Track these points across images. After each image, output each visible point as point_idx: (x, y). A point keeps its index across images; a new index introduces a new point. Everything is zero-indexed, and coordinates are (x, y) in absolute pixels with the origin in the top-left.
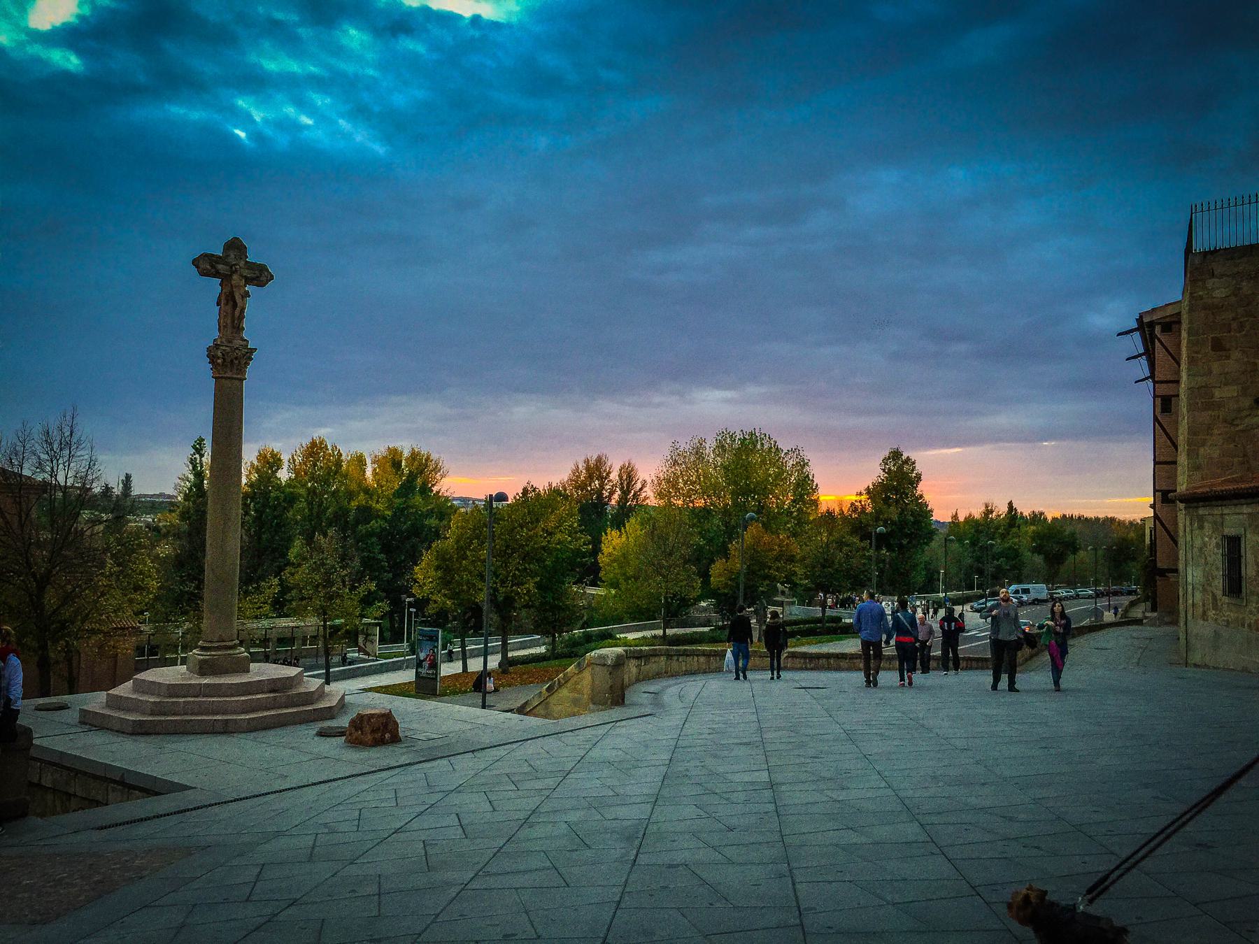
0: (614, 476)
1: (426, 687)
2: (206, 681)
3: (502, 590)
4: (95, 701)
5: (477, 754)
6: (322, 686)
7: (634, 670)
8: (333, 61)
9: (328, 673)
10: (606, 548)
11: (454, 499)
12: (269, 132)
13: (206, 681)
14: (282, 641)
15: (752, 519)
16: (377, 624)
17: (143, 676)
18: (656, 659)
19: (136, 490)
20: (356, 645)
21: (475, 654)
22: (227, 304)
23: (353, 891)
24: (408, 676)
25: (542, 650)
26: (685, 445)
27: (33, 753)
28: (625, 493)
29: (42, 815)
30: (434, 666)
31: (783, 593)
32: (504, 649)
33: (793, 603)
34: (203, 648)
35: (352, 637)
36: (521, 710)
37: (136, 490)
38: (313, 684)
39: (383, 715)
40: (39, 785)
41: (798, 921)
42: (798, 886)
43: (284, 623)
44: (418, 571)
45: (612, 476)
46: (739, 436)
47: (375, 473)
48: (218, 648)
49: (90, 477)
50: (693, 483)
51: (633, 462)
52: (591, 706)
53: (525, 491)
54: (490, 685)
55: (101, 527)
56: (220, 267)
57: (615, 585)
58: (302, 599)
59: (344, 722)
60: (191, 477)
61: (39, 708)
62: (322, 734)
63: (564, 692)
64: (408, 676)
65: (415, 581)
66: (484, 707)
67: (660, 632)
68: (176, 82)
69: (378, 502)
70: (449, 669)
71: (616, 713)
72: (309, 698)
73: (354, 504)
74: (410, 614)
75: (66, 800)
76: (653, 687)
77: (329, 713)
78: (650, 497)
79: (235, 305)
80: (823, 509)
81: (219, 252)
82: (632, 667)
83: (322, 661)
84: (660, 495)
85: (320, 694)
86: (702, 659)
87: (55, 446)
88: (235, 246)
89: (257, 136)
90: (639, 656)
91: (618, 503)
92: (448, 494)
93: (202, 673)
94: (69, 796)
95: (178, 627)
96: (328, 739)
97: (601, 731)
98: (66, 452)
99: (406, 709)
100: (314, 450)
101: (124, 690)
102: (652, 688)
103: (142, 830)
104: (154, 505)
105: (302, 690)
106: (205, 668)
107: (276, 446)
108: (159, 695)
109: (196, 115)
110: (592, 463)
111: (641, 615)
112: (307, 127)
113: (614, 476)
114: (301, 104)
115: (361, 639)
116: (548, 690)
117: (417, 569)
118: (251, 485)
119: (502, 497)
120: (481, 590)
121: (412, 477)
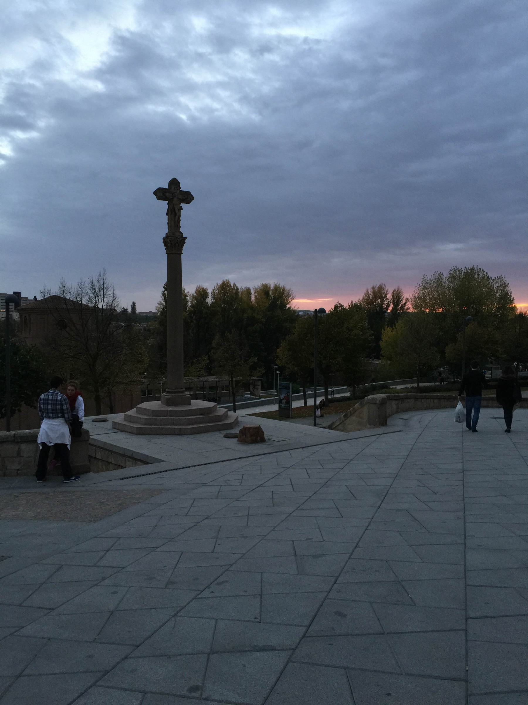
0: (389, 296)
1: (285, 413)
2: (170, 409)
3: (324, 362)
4: (119, 417)
5: (304, 449)
6: (227, 412)
7: (395, 407)
8: (230, 71)
9: (234, 405)
10: (384, 338)
11: (300, 311)
12: (197, 114)
13: (170, 409)
14: (211, 388)
15: (469, 320)
16: (259, 380)
17: (140, 406)
18: (408, 400)
19: (138, 311)
20: (249, 391)
21: (310, 396)
22: (172, 213)
23: (236, 514)
24: (275, 408)
25: (348, 394)
26: (430, 276)
27: (90, 442)
28: (396, 305)
29: (94, 472)
30: (288, 402)
31: (491, 363)
32: (326, 394)
33: (498, 368)
34: (168, 392)
35: (247, 386)
36: (330, 427)
37: (138, 311)
38: (221, 411)
39: (256, 428)
40: (95, 458)
41: (463, 542)
42: (467, 524)
43: (212, 379)
44: (279, 351)
45: (388, 296)
46: (464, 270)
47: (256, 298)
48: (175, 392)
49: (113, 305)
50: (435, 299)
51: (400, 288)
52: (368, 426)
53: (336, 307)
54: (318, 413)
55: (121, 331)
56: (167, 194)
57: (390, 358)
58: (220, 366)
59: (237, 431)
60: (164, 303)
61: (94, 421)
62: (227, 436)
63: (353, 418)
64: (275, 408)
65: (278, 357)
66: (315, 425)
67: (416, 385)
68: (149, 92)
69: (258, 314)
70: (296, 404)
71: (380, 430)
72: (220, 418)
73: (245, 315)
74: (276, 374)
75: (108, 465)
76: (405, 416)
77: (230, 426)
78: (410, 308)
79: (176, 214)
80: (518, 312)
81: (166, 186)
82: (393, 405)
83: (232, 399)
84: (415, 306)
85: (226, 416)
86: (436, 401)
87: (97, 290)
88: (174, 183)
89: (193, 118)
90: (398, 399)
91: (392, 311)
92: (295, 309)
93: (168, 405)
94: (109, 463)
95: (160, 380)
96: (230, 439)
97: (373, 438)
98: (102, 293)
99: (269, 426)
100: (225, 287)
101: (132, 412)
102: (405, 417)
103: (140, 480)
104: (147, 317)
105: (217, 414)
106: (169, 403)
107: (205, 285)
108: (148, 415)
109: (161, 109)
110: (376, 289)
111: (404, 375)
112: (217, 110)
113: (389, 296)
114: (214, 97)
115: (251, 387)
116: (344, 416)
117: (278, 350)
118: (193, 306)
119: (322, 311)
120: (313, 362)
121: (275, 299)
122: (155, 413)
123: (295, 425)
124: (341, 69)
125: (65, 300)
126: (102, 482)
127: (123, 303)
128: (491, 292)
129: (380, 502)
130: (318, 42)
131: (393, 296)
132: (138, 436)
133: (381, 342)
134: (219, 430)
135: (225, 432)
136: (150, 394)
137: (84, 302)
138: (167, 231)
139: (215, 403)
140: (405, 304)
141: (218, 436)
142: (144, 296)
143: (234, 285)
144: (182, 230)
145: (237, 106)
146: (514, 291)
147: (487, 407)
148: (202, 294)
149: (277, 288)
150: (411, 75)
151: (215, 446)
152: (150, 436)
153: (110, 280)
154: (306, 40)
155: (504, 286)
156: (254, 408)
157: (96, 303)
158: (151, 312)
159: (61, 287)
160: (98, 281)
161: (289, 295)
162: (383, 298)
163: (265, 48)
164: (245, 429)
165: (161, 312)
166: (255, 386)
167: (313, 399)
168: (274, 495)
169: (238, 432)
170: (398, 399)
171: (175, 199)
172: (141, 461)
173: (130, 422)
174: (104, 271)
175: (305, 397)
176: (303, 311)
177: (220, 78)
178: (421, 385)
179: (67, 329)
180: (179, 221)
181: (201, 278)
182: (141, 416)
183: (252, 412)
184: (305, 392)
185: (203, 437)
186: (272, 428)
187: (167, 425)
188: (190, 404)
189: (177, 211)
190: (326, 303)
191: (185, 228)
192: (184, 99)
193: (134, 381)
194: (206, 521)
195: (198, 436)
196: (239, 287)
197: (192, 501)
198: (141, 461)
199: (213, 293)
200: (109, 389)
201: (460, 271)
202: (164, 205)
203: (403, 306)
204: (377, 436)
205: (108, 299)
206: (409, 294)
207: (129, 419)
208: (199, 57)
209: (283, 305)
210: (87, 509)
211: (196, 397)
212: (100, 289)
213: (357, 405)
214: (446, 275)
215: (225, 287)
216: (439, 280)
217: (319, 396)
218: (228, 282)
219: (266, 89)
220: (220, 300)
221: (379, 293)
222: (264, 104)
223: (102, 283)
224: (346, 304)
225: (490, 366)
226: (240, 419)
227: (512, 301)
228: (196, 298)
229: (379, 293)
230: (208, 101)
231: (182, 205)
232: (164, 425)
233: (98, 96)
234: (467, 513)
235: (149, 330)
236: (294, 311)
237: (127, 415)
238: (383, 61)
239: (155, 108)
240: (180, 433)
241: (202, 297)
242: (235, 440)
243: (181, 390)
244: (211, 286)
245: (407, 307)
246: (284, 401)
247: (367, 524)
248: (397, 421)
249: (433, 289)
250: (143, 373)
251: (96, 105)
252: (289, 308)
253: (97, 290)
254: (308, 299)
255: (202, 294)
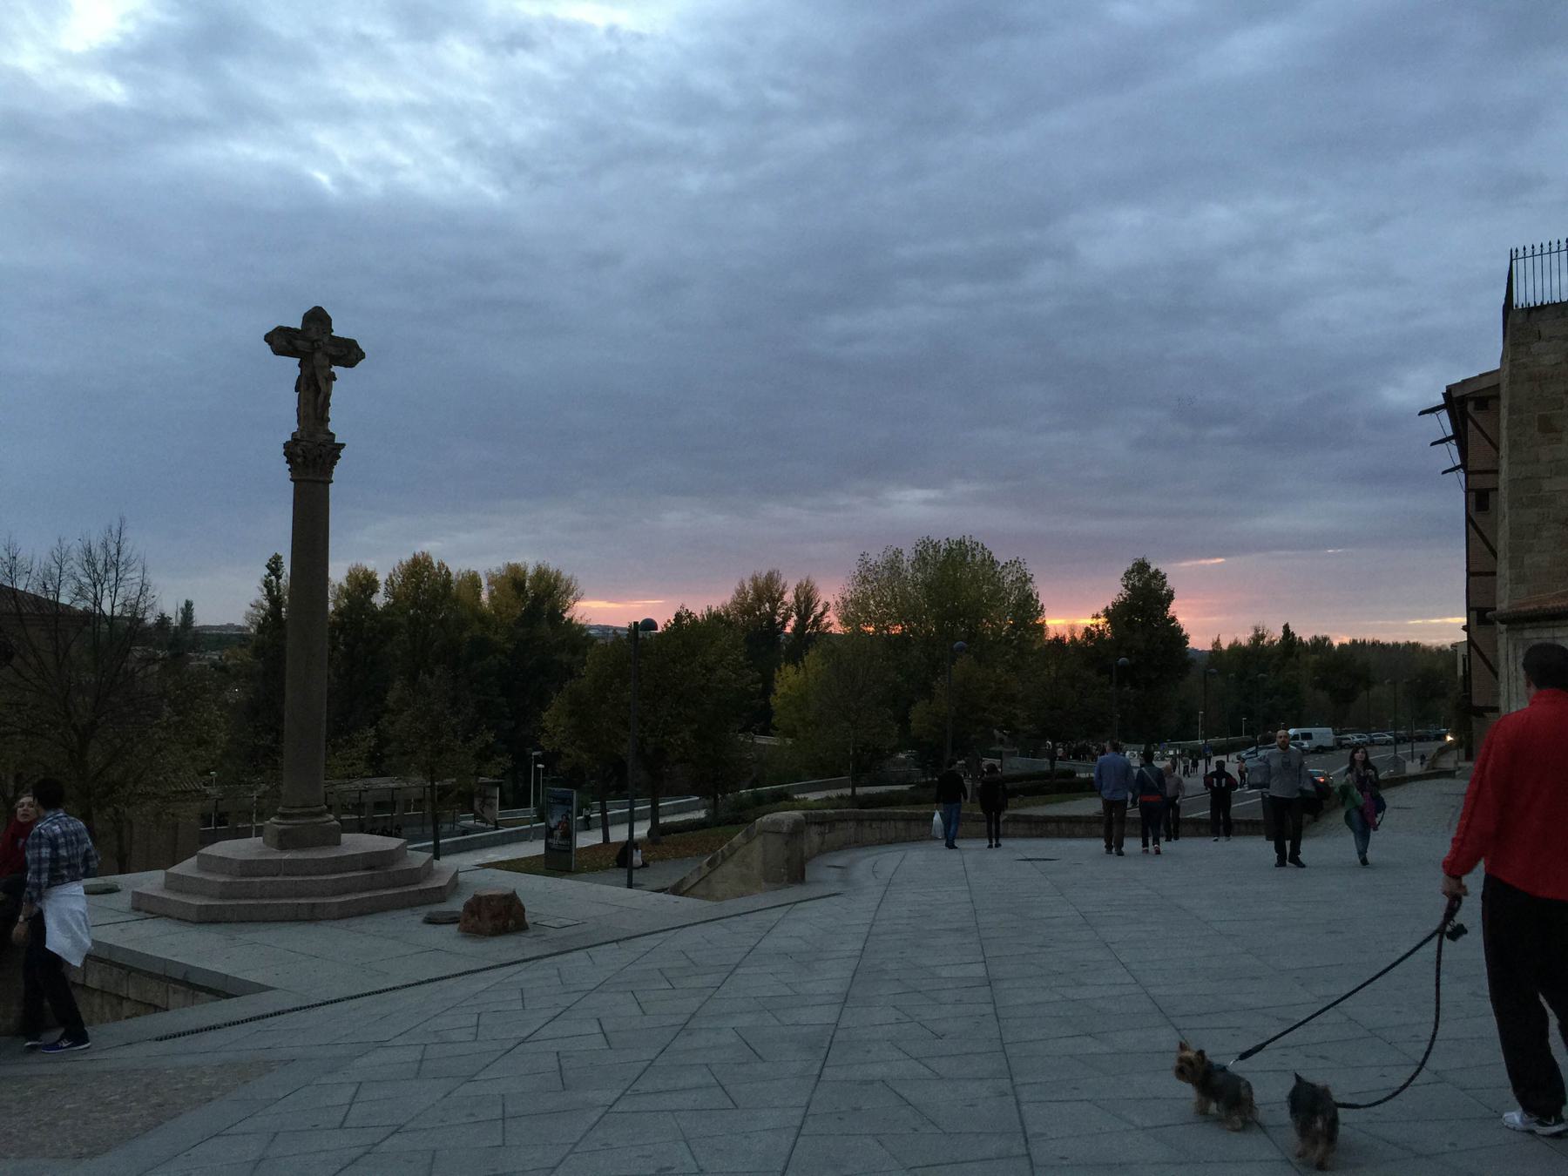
0: (789, 597)
1: (559, 861)
2: (287, 856)
3: (650, 740)
4: (150, 881)
6: (429, 862)
7: (816, 839)
10: (780, 688)
11: (591, 627)
12: (357, 175)
13: (287, 856)
14: (379, 806)
15: (961, 649)
20: (472, 810)
21: (619, 820)
24: (537, 848)
25: (701, 814)
26: (876, 556)
28: (803, 618)
30: (568, 836)
31: (1001, 741)
32: (655, 814)
33: (1013, 754)
34: (283, 816)
35: (466, 800)
36: (676, 890)
39: (506, 897)
47: (492, 596)
49: (141, 606)
50: (887, 605)
51: (812, 580)
53: (678, 617)
54: (637, 858)
55: (156, 668)
56: (299, 343)
57: (791, 733)
58: (404, 754)
59: (457, 905)
60: (266, 604)
62: (431, 921)
64: (537, 848)
65: (543, 730)
66: (630, 886)
67: (848, 792)
68: (240, 113)
69: (496, 632)
70: (587, 839)
72: (415, 876)
74: (537, 770)
76: (841, 859)
77: (440, 895)
79: (318, 390)
80: (1051, 635)
81: (297, 324)
82: (813, 836)
83: (429, 830)
84: (846, 620)
87: (100, 567)
89: (345, 182)
90: (822, 822)
91: (794, 630)
93: (283, 847)
94: (121, 999)
95: (252, 790)
97: (776, 914)
98: (112, 575)
99: (535, 891)
100: (418, 569)
101: (187, 867)
104: (222, 638)
106: (285, 841)
107: (370, 565)
110: (761, 581)
111: (824, 771)
113: (789, 597)
114: (395, 138)
115: (477, 803)
116: (709, 864)
117: (545, 715)
118: (340, 612)
119: (649, 624)
121: (538, 600)
122: (248, 868)
123: (594, 887)
124: (691, 106)
125: (14, 591)
126: (120, 1047)
127: (166, 603)
128: (998, 594)
129: (819, 1065)
130: (640, 37)
131: (797, 597)
132: (201, 927)
133: (772, 698)
134: (411, 905)
135: (425, 911)
136: (223, 824)
137: (64, 600)
138: (295, 427)
139: (402, 841)
140: (823, 614)
141: (410, 921)
142: (216, 584)
143: (441, 565)
144: (331, 427)
145: (450, 163)
146: (1044, 591)
147: (1014, 836)
148: (363, 584)
149: (541, 574)
150: (833, 132)
151: (400, 945)
152: (233, 926)
153: (134, 544)
154: (612, 32)
155: (1025, 580)
156: (484, 852)
157: (97, 602)
158: (230, 626)
159: (6, 559)
160: (105, 546)
161: (568, 591)
162: (775, 600)
163: (517, 39)
164: (478, 900)
165: (259, 626)
166: (486, 799)
167: (627, 827)
168: (563, 1061)
169: (460, 909)
170: (822, 822)
171: (318, 355)
172: (209, 991)
173: (179, 891)
174: (122, 521)
175: (605, 825)
176: (597, 627)
177: (410, 95)
178: (860, 791)
179: (16, 661)
180: (326, 405)
181: (368, 547)
182: (209, 877)
183: (480, 861)
184: (604, 811)
185: (370, 924)
186: (541, 894)
187: (279, 897)
188: (338, 843)
189: (322, 384)
190: (658, 608)
191: (339, 423)
192: (325, 137)
193: (184, 792)
194: (395, 1140)
195: (357, 921)
196: (454, 570)
197: (354, 1089)
198: (209, 991)
199: (390, 582)
200: (117, 811)
201: (936, 547)
202: (290, 367)
203: (817, 621)
204: (785, 909)
205: (129, 590)
206: (832, 595)
207: (174, 883)
208: (364, 42)
209: (556, 616)
210: (69, 1122)
211: (361, 828)
212: (106, 565)
213: (738, 838)
214: (909, 554)
215: (418, 569)
216: (893, 566)
217: (640, 819)
218: (427, 558)
219: (519, 132)
220: (407, 598)
221: (767, 591)
222: (514, 164)
223: (113, 551)
224: (699, 607)
225: (998, 748)
226: (461, 877)
227: (1040, 612)
228: (348, 594)
229: (767, 591)
230: (383, 148)
231: (334, 369)
232: (271, 897)
233: (107, 110)
234: (1018, 1080)
235: (223, 669)
236: (582, 628)
237: (178, 877)
238: (775, 96)
239: (247, 154)
240: (312, 916)
241: (364, 591)
242: (453, 929)
243: (317, 809)
244: (385, 566)
245: (826, 620)
246: (557, 833)
247: (797, 1123)
248: (823, 871)
249: (881, 584)
250: (207, 772)
251: (102, 133)
252: (570, 620)
253: (100, 567)
254: (616, 602)
255: (363, 584)
